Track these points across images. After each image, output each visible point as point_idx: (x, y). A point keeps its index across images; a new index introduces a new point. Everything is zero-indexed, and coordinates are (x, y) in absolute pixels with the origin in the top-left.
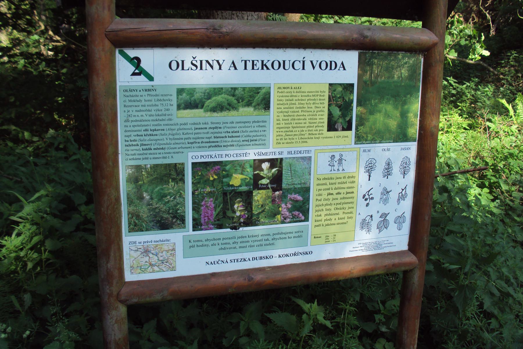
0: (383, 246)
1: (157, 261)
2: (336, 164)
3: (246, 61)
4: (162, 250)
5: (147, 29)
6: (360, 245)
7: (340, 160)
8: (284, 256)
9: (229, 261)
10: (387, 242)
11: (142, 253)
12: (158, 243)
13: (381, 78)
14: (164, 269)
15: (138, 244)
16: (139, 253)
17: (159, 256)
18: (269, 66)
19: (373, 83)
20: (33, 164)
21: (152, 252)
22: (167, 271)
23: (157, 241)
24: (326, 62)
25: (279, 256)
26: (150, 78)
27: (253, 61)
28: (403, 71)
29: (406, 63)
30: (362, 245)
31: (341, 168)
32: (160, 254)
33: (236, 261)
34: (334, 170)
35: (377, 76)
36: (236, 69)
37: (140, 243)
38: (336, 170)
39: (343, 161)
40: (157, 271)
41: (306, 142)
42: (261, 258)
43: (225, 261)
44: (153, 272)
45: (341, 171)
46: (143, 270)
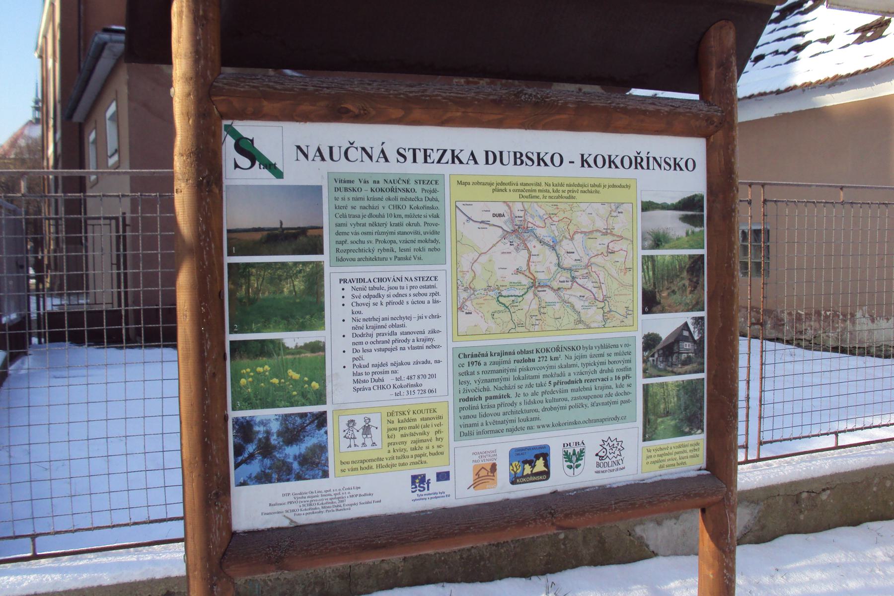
0: (348, 501)
2: (359, 435)
3: (414, 150)
4: (572, 228)
7: (367, 430)
8: (626, 162)
11: (505, 235)
13: (264, 293)
17: (562, 252)
19: (252, 301)
21: (540, 232)
25: (584, 161)
26: (279, 174)
27: (425, 150)
28: (296, 283)
29: (300, 272)
31: (369, 442)
32: (566, 245)
33: (420, 156)
34: (355, 445)
35: (257, 291)
43: (376, 154)
45: (369, 446)
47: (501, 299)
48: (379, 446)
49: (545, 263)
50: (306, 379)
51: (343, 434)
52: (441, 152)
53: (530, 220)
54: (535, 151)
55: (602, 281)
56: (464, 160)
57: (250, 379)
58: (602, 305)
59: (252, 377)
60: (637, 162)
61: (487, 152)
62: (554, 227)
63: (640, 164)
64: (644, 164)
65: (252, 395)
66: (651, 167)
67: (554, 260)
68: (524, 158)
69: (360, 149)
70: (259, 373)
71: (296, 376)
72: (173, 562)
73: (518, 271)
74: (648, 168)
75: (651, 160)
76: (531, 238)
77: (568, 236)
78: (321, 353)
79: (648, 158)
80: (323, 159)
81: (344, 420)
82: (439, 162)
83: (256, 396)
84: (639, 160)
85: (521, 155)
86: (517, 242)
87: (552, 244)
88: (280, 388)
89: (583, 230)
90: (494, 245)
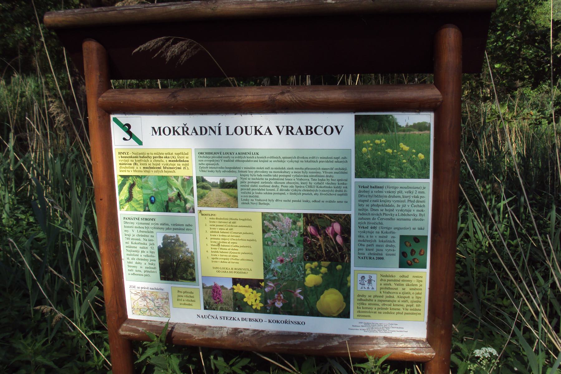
0: (391, 329)
2: (366, 283)
5: (157, 94)
6: (361, 325)
7: (370, 281)
9: (219, 318)
10: (396, 326)
14: (160, 315)
20: (154, 356)
21: (150, 297)
24: (326, 133)
25: (269, 321)
26: (140, 143)
30: (363, 324)
32: (156, 301)
33: (225, 318)
36: (271, 134)
37: (139, 288)
40: (154, 316)
41: (269, 204)
44: (151, 315)
48: (375, 290)
50: (414, 151)
51: (359, 282)
57: (370, 149)
59: (371, 147)
63: (186, 132)
65: (371, 160)
70: (377, 144)
71: (406, 148)
72: (181, 158)
78: (427, 132)
81: (360, 276)
83: (374, 161)
84: (185, 129)
88: (393, 156)
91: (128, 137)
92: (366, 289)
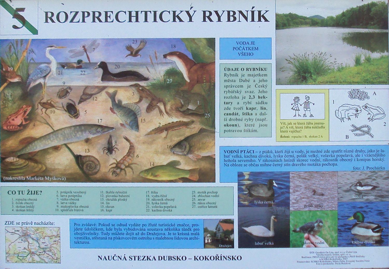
0: (350, 259)
1: (37, 248)
2: (302, 108)
3: (146, 13)
4: (44, 235)
6: (312, 255)
7: (307, 104)
9: (128, 258)
10: (355, 254)
11: (20, 237)
12: (39, 226)
15: (15, 225)
16: (16, 236)
17: (40, 243)
18: (54, 18)
22: (50, 262)
23: (38, 224)
25: (195, 258)
26: (35, 31)
31: (308, 114)
33: (137, 258)
37: (18, 224)
38: (302, 115)
39: (311, 105)
42: (170, 258)
45: (308, 117)
46: (21, 258)
47: (19, 257)
49: (34, 246)
52: (143, 257)
53: (29, 232)
54: (176, 256)
55: (56, 253)
56: (151, 259)
58: (56, 261)
60: (216, 258)
61: (159, 257)
62: (37, 234)
63: (218, 259)
64: (220, 258)
66: (222, 259)
67: (38, 245)
68: (172, 258)
69: (117, 257)
73: (25, 248)
74: (221, 260)
75: (222, 257)
76: (29, 238)
77: (42, 237)
79: (221, 257)
80: (106, 260)
82: (143, 260)
84: (217, 257)
85: (171, 257)
86: (24, 239)
87: (36, 240)
89: (48, 235)
90: (16, 240)
91: (19, 24)
92: (302, 118)
